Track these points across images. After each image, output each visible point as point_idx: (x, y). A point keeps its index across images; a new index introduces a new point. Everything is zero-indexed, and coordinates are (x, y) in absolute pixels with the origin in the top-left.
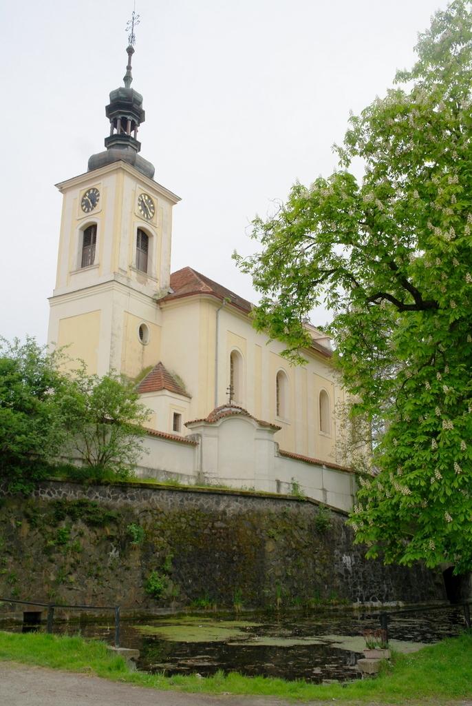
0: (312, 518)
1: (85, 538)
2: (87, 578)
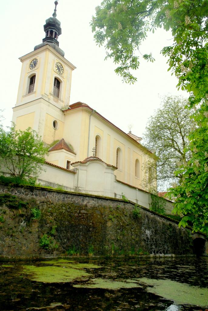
0: (131, 211)
1: (7, 214)
2: (6, 236)
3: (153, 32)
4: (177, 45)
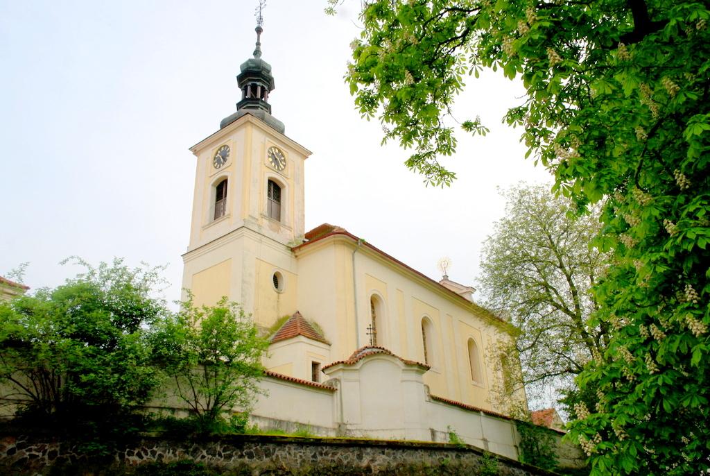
3: (477, 75)
4: (535, 102)
